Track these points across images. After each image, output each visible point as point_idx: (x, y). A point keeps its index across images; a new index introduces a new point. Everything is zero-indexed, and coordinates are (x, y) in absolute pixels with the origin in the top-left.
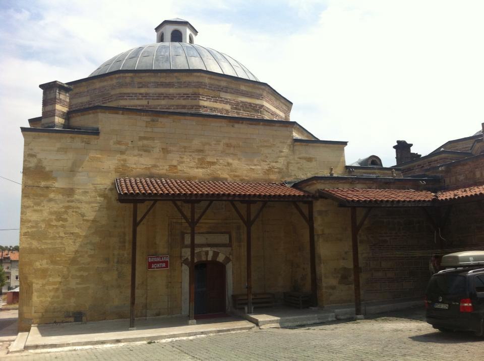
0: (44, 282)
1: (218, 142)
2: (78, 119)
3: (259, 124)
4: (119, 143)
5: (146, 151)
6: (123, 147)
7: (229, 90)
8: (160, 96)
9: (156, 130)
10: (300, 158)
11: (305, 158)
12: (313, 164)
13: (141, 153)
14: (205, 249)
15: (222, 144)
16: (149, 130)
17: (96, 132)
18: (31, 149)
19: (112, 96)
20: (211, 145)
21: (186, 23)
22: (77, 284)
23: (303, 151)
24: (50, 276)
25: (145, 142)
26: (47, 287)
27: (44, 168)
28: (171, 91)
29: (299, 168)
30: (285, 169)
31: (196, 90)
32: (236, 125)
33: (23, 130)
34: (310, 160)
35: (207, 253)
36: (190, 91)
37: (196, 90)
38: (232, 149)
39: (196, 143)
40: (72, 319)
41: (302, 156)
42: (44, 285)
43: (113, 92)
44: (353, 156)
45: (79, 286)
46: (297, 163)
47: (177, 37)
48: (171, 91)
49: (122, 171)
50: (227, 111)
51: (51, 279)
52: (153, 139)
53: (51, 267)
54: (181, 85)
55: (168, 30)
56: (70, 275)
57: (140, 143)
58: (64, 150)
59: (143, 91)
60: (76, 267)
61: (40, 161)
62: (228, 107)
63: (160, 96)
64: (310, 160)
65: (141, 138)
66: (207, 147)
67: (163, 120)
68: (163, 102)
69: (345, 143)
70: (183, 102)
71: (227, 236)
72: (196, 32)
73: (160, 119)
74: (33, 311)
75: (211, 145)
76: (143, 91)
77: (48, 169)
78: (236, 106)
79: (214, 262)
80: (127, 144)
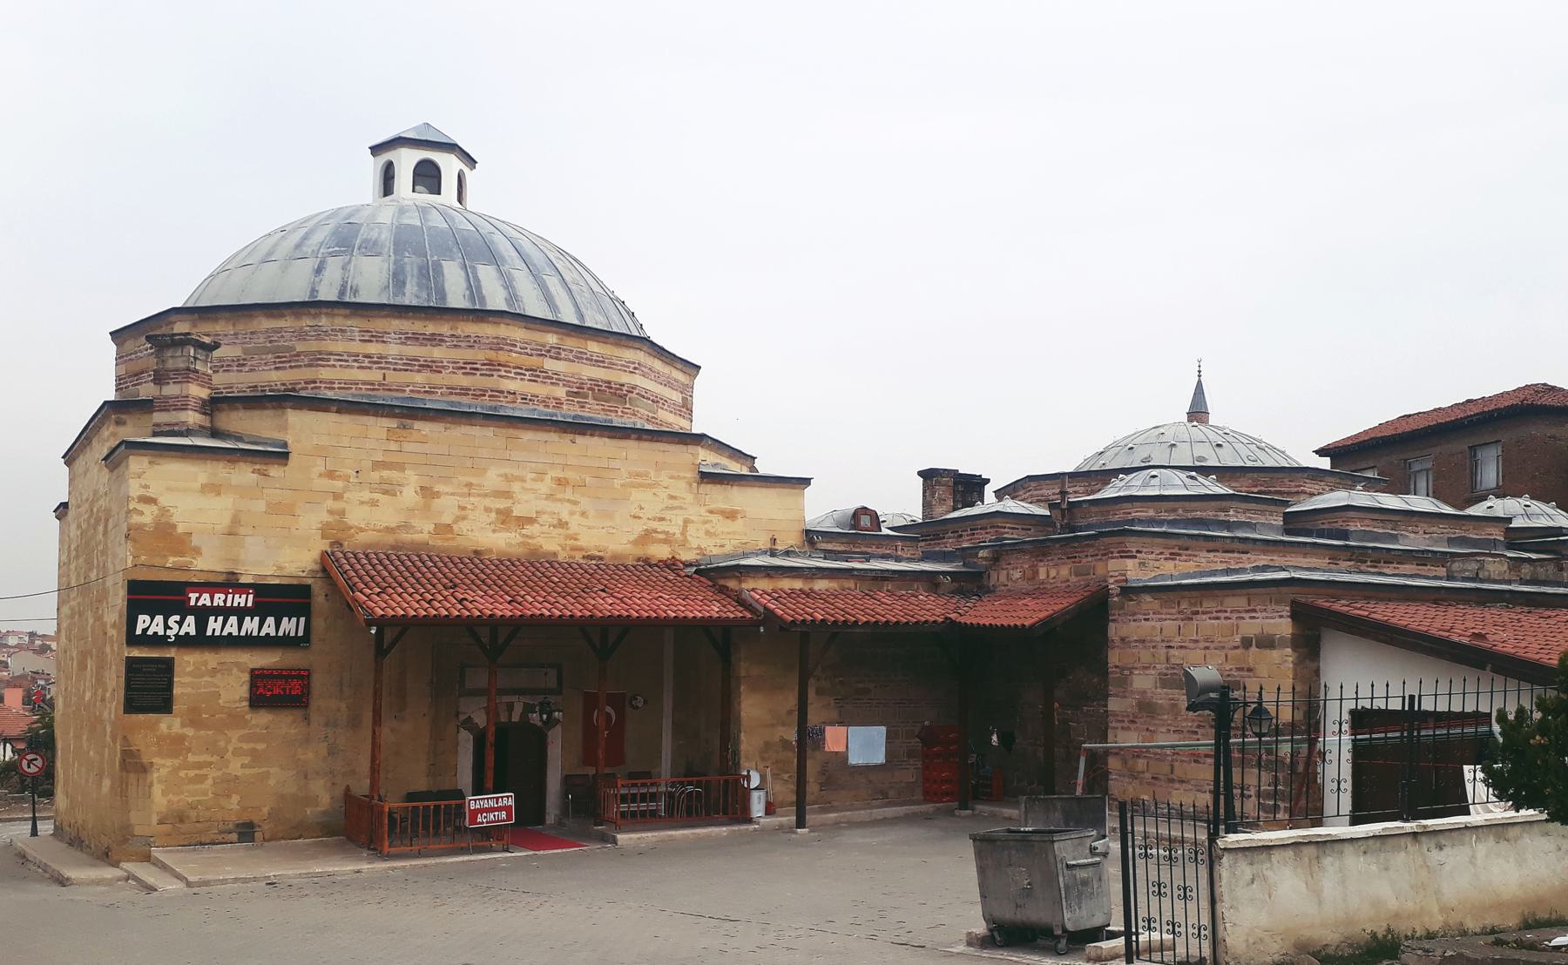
0: (177, 762)
1: (541, 475)
2: (234, 415)
3: (627, 437)
4: (331, 475)
5: (386, 492)
6: (338, 485)
7: (563, 354)
8: (411, 364)
9: (408, 447)
10: (711, 512)
11: (722, 512)
12: (738, 525)
13: (377, 496)
14: (506, 699)
15: (548, 478)
16: (393, 446)
17: (283, 457)
18: (146, 487)
19: (298, 355)
20: (523, 481)
21: (451, 148)
22: (243, 766)
23: (719, 496)
24: (189, 750)
25: (386, 473)
26: (182, 774)
27: (174, 527)
28: (437, 353)
29: (707, 533)
30: (678, 535)
31: (492, 355)
32: (580, 440)
33: (972, 941)
34: (731, 515)
35: (510, 707)
36: (480, 355)
37: (492, 355)
38: (569, 490)
39: (492, 478)
40: (234, 836)
41: (712, 506)
42: (176, 770)
43: (300, 347)
44: (822, 507)
45: (248, 771)
46: (705, 522)
47: (428, 176)
48: (437, 353)
49: (336, 533)
50: (559, 403)
51: (191, 758)
52: (401, 467)
53: (190, 732)
54: (457, 342)
55: (405, 162)
56: (231, 749)
57: (376, 476)
58: (213, 489)
59: (373, 348)
60: (243, 732)
61: (164, 511)
62: (561, 392)
63: (411, 364)
64: (731, 515)
65: (377, 465)
66: (516, 487)
67: (424, 428)
68: (419, 378)
69: (806, 482)
70: (463, 381)
71: (553, 673)
72: (471, 161)
73: (418, 425)
74: (155, 819)
75: (523, 481)
76: (373, 348)
77: (180, 529)
78: (578, 392)
79: (525, 724)
80: (347, 479)
